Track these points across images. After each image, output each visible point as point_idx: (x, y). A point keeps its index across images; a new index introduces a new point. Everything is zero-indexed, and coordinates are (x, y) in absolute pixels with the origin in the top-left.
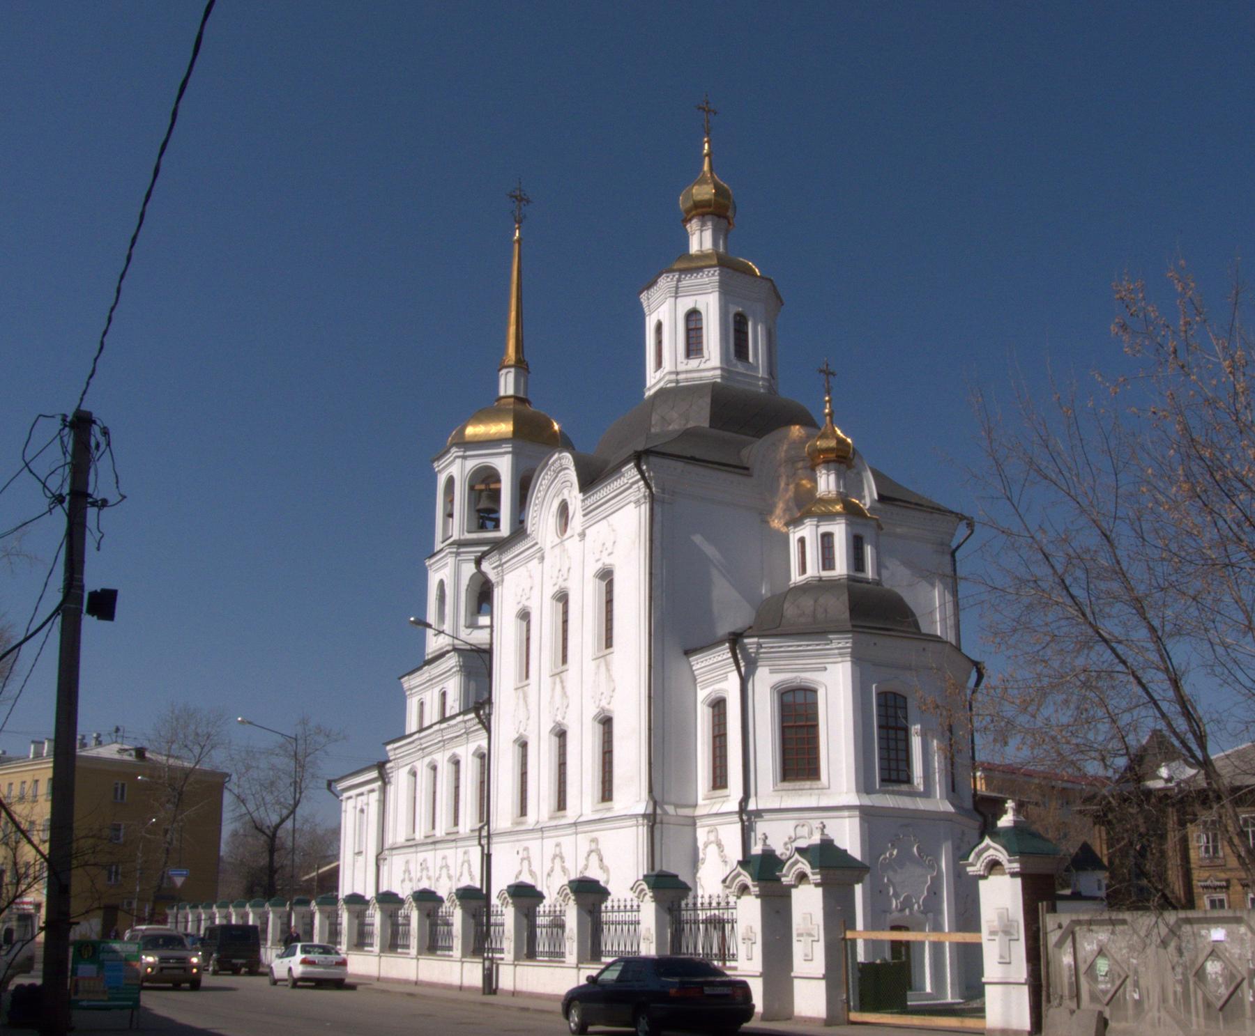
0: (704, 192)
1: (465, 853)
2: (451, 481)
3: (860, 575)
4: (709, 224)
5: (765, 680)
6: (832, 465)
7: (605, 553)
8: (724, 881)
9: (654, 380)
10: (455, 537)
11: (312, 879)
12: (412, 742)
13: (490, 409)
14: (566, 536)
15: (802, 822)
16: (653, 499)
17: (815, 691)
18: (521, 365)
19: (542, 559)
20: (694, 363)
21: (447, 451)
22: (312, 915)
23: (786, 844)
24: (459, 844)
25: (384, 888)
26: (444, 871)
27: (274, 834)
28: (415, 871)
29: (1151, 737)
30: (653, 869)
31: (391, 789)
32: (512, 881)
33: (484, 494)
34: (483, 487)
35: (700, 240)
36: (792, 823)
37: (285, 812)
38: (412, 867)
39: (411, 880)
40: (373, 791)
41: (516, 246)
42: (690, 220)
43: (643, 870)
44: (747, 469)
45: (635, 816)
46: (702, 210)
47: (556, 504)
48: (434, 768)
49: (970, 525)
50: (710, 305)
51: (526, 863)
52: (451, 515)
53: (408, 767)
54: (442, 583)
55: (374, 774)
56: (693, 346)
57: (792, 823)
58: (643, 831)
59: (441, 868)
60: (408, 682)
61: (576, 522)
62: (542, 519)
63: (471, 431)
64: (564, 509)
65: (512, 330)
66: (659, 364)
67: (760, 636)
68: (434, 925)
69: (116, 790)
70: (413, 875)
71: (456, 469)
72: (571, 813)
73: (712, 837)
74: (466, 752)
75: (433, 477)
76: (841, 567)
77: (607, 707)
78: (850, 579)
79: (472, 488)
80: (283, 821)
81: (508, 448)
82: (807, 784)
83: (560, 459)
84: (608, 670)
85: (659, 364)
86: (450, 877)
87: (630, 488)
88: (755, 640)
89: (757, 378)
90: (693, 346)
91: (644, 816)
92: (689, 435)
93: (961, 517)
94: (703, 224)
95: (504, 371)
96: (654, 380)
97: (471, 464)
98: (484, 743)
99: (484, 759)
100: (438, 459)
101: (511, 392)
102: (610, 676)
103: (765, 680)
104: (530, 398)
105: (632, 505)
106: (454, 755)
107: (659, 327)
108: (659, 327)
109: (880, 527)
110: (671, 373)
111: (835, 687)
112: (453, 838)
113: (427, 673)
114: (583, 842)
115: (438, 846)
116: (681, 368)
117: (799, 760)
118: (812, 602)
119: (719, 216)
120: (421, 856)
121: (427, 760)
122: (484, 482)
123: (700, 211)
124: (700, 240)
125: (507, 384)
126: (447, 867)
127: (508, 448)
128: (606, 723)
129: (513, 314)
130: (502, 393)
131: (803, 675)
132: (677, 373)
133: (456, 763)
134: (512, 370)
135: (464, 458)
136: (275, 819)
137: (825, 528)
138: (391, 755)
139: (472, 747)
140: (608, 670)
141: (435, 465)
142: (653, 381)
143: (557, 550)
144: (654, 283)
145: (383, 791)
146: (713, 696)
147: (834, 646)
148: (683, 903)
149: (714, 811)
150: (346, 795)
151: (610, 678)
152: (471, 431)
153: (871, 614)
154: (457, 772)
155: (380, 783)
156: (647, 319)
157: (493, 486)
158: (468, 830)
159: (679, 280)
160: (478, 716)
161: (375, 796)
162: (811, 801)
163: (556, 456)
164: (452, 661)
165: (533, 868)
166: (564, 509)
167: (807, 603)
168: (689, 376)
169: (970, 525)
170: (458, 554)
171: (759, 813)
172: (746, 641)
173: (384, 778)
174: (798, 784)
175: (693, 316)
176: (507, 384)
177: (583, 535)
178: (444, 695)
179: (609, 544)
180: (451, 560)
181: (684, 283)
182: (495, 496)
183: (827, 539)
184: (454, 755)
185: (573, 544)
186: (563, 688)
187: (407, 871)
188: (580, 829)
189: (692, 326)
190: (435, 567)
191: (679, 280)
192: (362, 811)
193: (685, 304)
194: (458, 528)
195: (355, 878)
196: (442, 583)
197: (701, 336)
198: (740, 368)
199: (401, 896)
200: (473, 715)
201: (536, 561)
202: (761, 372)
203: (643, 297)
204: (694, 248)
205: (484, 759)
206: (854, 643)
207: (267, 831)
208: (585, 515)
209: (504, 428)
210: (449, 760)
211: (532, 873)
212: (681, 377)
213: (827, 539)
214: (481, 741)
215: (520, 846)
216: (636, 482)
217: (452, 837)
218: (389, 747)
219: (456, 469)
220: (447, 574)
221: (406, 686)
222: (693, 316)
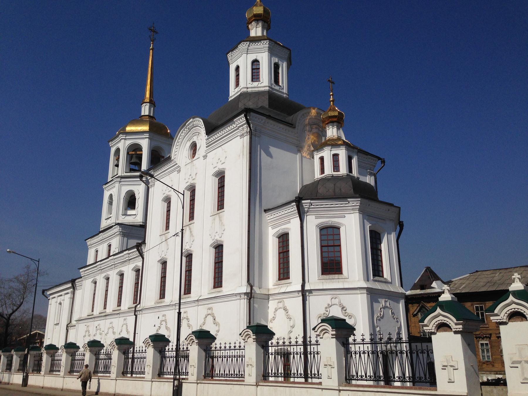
0: (258, 10)
1: (125, 320)
2: (118, 150)
3: (351, 174)
4: (260, 24)
5: (313, 223)
6: (335, 124)
8: (240, 334)
9: (233, 92)
10: (119, 174)
11: (24, 339)
12: (96, 267)
13: (139, 120)
14: (195, 158)
15: (335, 296)
16: (251, 134)
17: (339, 228)
18: (152, 102)
19: (179, 171)
20: (255, 84)
21: (118, 136)
22: (12, 356)
23: (326, 308)
24: (121, 315)
25: (70, 340)
26: (111, 330)
27: (9, 318)
28: (92, 331)
29: (426, 271)
30: (250, 323)
31: (78, 293)
32: (153, 332)
33: (134, 156)
34: (134, 153)
35: (256, 31)
36: (329, 297)
37: (15, 308)
38: (91, 329)
40: (68, 293)
41: (151, 51)
42: (251, 23)
43: (244, 325)
44: (292, 125)
45: (240, 294)
46: (257, 18)
47: (189, 144)
48: (108, 279)
49: (383, 162)
50: (264, 58)
52: (117, 166)
54: (111, 196)
55: (70, 285)
56: (255, 76)
57: (329, 297)
58: (244, 303)
59: (109, 328)
60: (89, 242)
61: (200, 152)
62: (180, 152)
63: (129, 129)
64: (194, 147)
65: (148, 87)
66: (237, 84)
67: (311, 199)
68: (53, 360)
71: (122, 144)
72: (227, 287)
73: (281, 305)
75: (109, 149)
76: (343, 170)
77: (219, 239)
78: (348, 175)
79: (128, 153)
80: (14, 312)
81: (147, 135)
82: (336, 276)
83: (193, 122)
84: (220, 220)
85: (237, 84)
86: (114, 333)
88: (309, 201)
89: (283, 93)
90: (255, 76)
91: (246, 294)
92: (262, 108)
93: (379, 158)
94: (258, 24)
95: (144, 104)
96: (233, 92)
97: (128, 142)
98: (140, 264)
99: (139, 272)
100: (112, 141)
101: (147, 113)
102: (222, 223)
103: (313, 223)
104: (155, 117)
107: (238, 68)
108: (238, 68)
111: (351, 226)
112: (116, 313)
113: (102, 236)
114: (202, 310)
115: (107, 317)
116: (249, 86)
117: (331, 265)
118: (333, 185)
119: (265, 22)
120: (96, 323)
121: (104, 275)
122: (134, 153)
124: (256, 31)
125: (145, 110)
126: (113, 328)
127: (147, 135)
128: (219, 248)
129: (149, 81)
130: (143, 114)
132: (247, 88)
133: (122, 275)
134: (148, 104)
135: (125, 139)
136: (10, 311)
137: (335, 151)
138: (82, 274)
139: (132, 266)
140: (220, 220)
141: (110, 143)
142: (233, 93)
143: (189, 166)
144: (236, 47)
145: (74, 293)
146: (281, 231)
147: (350, 205)
148: (167, 348)
149: (283, 290)
150: (51, 297)
151: (222, 224)
152: (129, 129)
153: (363, 192)
155: (72, 290)
156: (230, 66)
157: (138, 153)
158: (126, 308)
159: (249, 46)
160: (138, 250)
161: (69, 296)
163: (191, 120)
164: (117, 229)
165: (168, 326)
166: (194, 147)
167: (330, 185)
168: (253, 89)
169: (383, 162)
170: (120, 182)
171: (310, 291)
172: (303, 202)
173: (74, 287)
174: (331, 276)
175: (255, 62)
176: (145, 110)
177: (205, 157)
178: (110, 246)
180: (117, 185)
181: (251, 47)
182: (140, 157)
183: (336, 157)
185: (199, 160)
186: (191, 232)
188: (200, 303)
189: (254, 67)
190: (107, 189)
191: (249, 46)
192: (60, 304)
193: (252, 57)
194: (121, 171)
195: (54, 335)
196: (111, 196)
197: (259, 72)
198: (277, 88)
199: (57, 346)
200: (136, 250)
202: (285, 91)
203: (229, 56)
204: (253, 34)
205: (139, 272)
206: (361, 203)
207: (6, 317)
208: (207, 147)
209: (146, 128)
211: (167, 328)
212: (248, 90)
213: (336, 157)
214: (138, 263)
215: (160, 314)
217: (118, 312)
218: (81, 270)
219: (122, 144)
220: (115, 192)
221: (88, 243)
222: (255, 62)
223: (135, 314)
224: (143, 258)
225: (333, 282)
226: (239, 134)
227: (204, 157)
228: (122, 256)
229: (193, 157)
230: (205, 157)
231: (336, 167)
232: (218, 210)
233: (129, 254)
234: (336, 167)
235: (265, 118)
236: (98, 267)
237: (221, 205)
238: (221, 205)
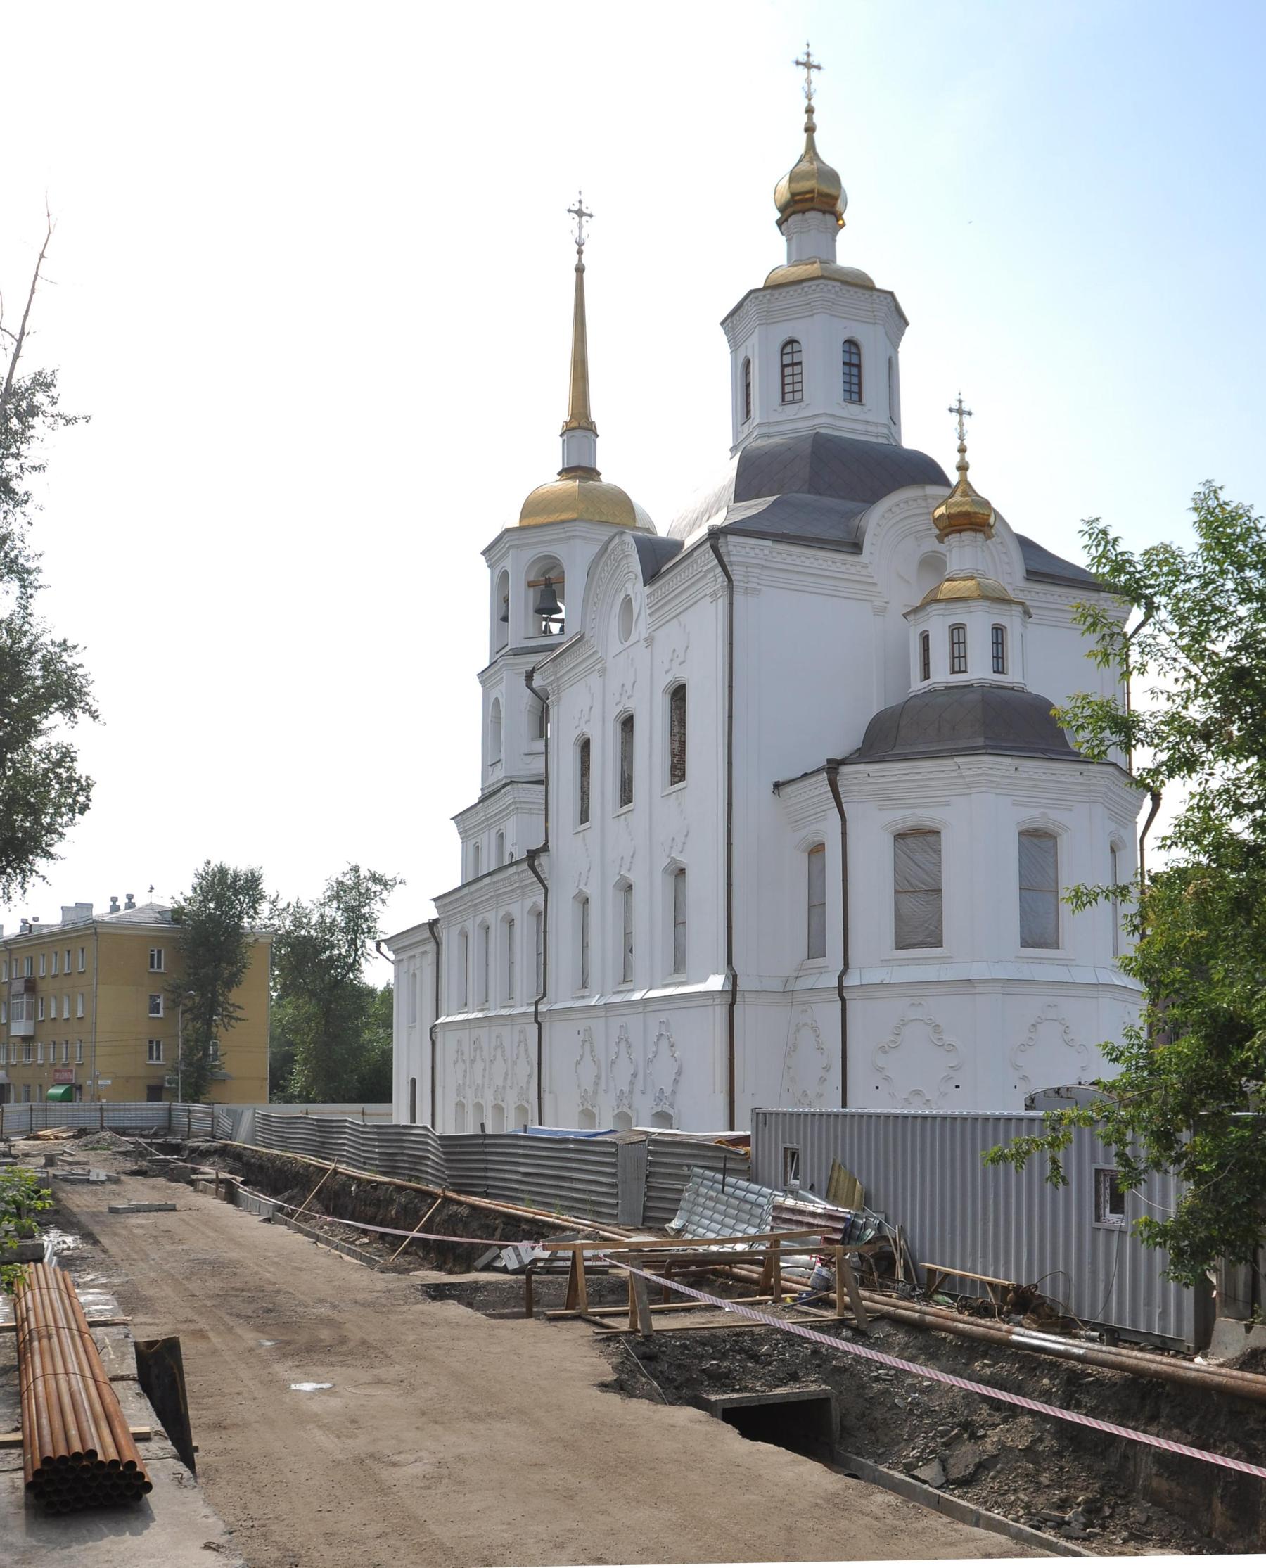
1: (521, 1032)
7: (584, 720)
19: (603, 672)
20: (791, 410)
39: (464, 1061)
47: (619, 602)
48: (511, 922)
51: (587, 1046)
53: (459, 926)
59: (495, 1049)
61: (641, 629)
69: (152, 956)
70: (466, 1057)
74: (520, 909)
87: (704, 576)
99: (542, 917)
105: (708, 599)
106: (508, 914)
109: (1027, 614)
110: (759, 425)
123: (799, 207)
131: (919, 812)
139: (528, 903)
154: (628, 905)
160: (532, 867)
162: (930, 973)
177: (650, 641)
179: (628, 687)
183: (957, 631)
184: (508, 914)
187: (460, 1051)
192: (414, 975)
201: (596, 674)
210: (460, 934)
213: (957, 631)
216: (712, 569)
223: (536, 1021)
224: (438, 944)
225: (918, 967)
226: (708, 591)
227: (646, 640)
228: (505, 879)
229: (627, 637)
230: (650, 641)
231: (958, 661)
232: (673, 783)
233: (471, 894)
234: (958, 661)
235: (769, 543)
236: (467, 899)
237: (584, 816)
238: (584, 816)
